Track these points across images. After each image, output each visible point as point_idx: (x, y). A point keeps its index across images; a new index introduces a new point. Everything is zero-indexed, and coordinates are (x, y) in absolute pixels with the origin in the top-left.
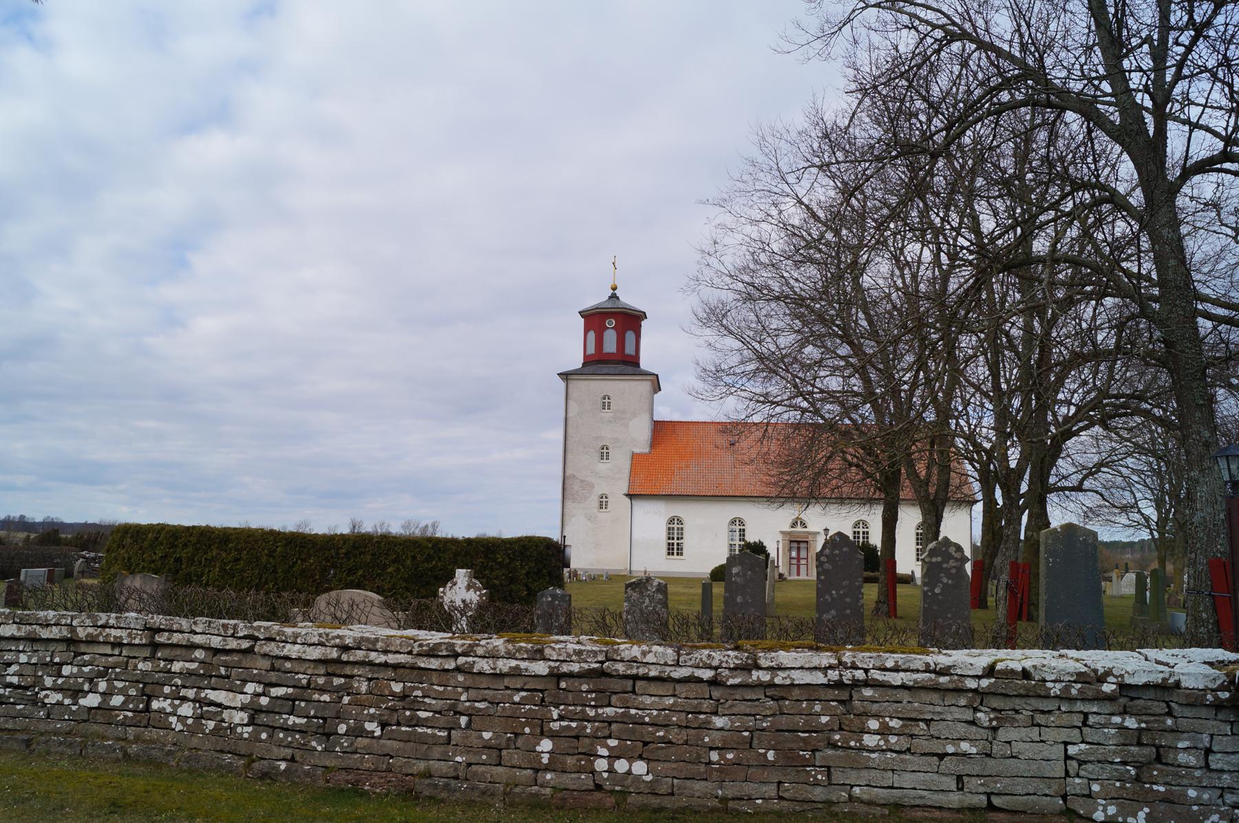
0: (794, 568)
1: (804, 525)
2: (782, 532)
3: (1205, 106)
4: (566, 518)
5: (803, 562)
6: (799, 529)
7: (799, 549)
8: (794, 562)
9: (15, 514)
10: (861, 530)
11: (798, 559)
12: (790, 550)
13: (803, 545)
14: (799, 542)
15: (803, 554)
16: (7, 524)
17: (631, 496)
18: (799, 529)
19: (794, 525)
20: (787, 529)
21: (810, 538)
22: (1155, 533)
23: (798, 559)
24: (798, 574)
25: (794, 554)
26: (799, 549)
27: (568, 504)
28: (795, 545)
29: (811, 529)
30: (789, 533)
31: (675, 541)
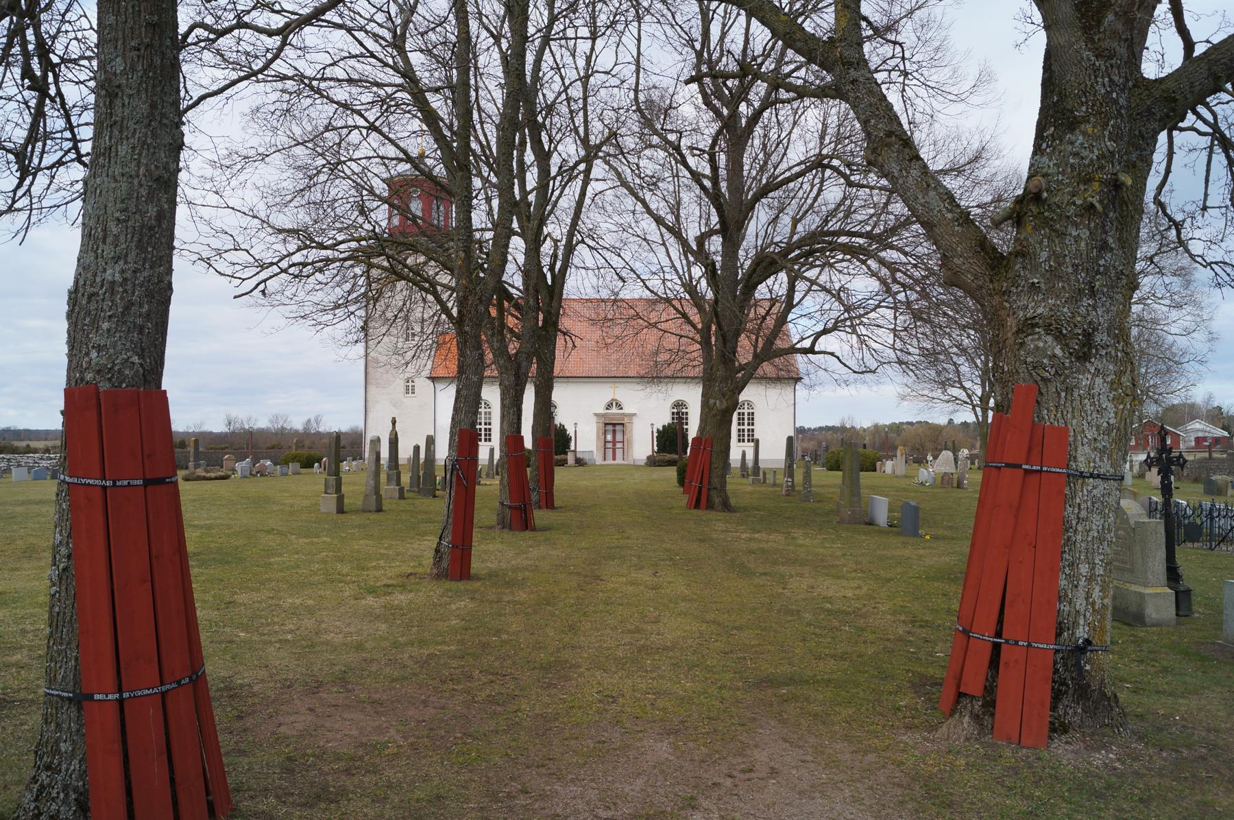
0: (610, 452)
1: (619, 406)
2: (596, 414)
3: (576, 38)
4: (370, 405)
5: (619, 445)
6: (614, 410)
7: (614, 431)
8: (609, 445)
9: (823, 425)
10: (746, 411)
11: (614, 442)
12: (605, 433)
13: (618, 428)
14: (614, 425)
15: (619, 437)
16: (7, 431)
17: (433, 379)
18: (614, 410)
19: (609, 406)
20: (602, 410)
21: (626, 420)
22: (991, 414)
23: (614, 442)
24: (614, 459)
25: (609, 437)
26: (614, 431)
27: (371, 389)
28: (610, 428)
29: (626, 410)
30: (604, 415)
31: (746, 427)
